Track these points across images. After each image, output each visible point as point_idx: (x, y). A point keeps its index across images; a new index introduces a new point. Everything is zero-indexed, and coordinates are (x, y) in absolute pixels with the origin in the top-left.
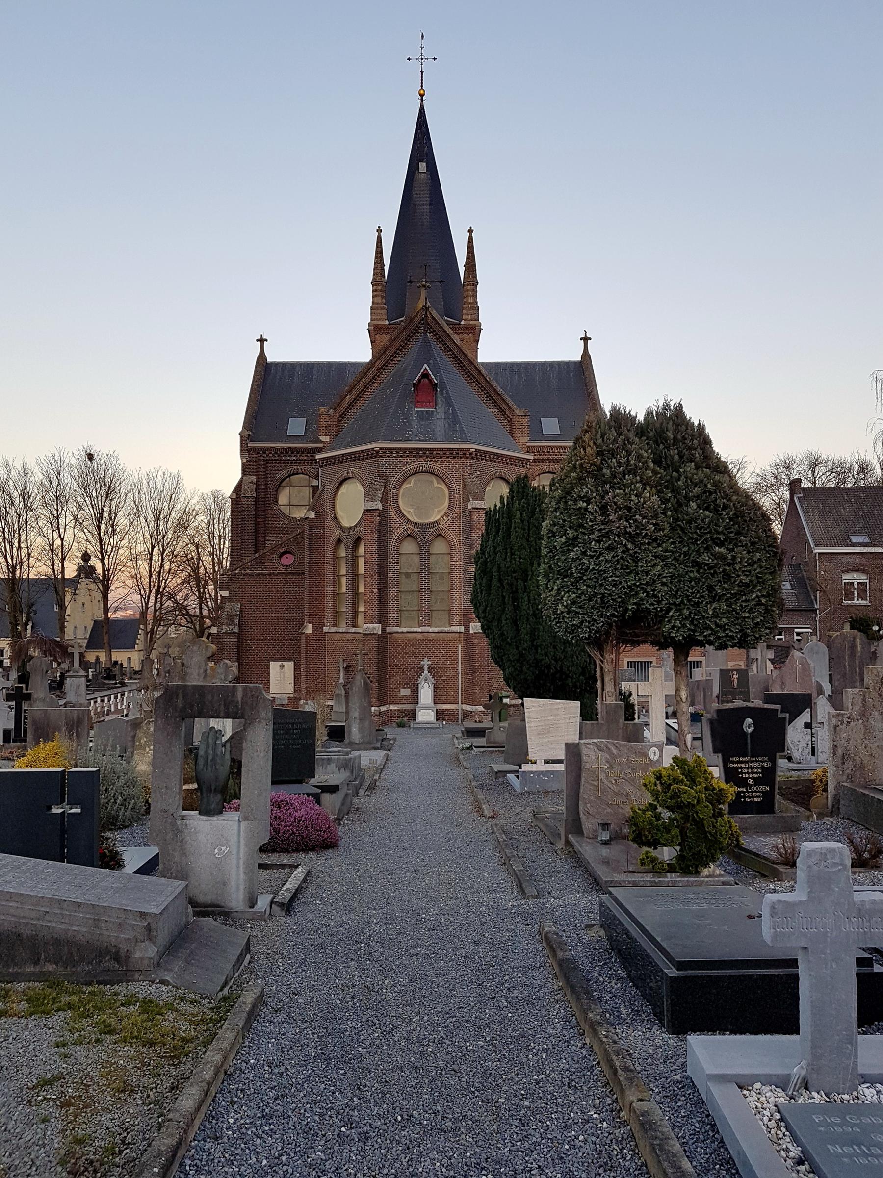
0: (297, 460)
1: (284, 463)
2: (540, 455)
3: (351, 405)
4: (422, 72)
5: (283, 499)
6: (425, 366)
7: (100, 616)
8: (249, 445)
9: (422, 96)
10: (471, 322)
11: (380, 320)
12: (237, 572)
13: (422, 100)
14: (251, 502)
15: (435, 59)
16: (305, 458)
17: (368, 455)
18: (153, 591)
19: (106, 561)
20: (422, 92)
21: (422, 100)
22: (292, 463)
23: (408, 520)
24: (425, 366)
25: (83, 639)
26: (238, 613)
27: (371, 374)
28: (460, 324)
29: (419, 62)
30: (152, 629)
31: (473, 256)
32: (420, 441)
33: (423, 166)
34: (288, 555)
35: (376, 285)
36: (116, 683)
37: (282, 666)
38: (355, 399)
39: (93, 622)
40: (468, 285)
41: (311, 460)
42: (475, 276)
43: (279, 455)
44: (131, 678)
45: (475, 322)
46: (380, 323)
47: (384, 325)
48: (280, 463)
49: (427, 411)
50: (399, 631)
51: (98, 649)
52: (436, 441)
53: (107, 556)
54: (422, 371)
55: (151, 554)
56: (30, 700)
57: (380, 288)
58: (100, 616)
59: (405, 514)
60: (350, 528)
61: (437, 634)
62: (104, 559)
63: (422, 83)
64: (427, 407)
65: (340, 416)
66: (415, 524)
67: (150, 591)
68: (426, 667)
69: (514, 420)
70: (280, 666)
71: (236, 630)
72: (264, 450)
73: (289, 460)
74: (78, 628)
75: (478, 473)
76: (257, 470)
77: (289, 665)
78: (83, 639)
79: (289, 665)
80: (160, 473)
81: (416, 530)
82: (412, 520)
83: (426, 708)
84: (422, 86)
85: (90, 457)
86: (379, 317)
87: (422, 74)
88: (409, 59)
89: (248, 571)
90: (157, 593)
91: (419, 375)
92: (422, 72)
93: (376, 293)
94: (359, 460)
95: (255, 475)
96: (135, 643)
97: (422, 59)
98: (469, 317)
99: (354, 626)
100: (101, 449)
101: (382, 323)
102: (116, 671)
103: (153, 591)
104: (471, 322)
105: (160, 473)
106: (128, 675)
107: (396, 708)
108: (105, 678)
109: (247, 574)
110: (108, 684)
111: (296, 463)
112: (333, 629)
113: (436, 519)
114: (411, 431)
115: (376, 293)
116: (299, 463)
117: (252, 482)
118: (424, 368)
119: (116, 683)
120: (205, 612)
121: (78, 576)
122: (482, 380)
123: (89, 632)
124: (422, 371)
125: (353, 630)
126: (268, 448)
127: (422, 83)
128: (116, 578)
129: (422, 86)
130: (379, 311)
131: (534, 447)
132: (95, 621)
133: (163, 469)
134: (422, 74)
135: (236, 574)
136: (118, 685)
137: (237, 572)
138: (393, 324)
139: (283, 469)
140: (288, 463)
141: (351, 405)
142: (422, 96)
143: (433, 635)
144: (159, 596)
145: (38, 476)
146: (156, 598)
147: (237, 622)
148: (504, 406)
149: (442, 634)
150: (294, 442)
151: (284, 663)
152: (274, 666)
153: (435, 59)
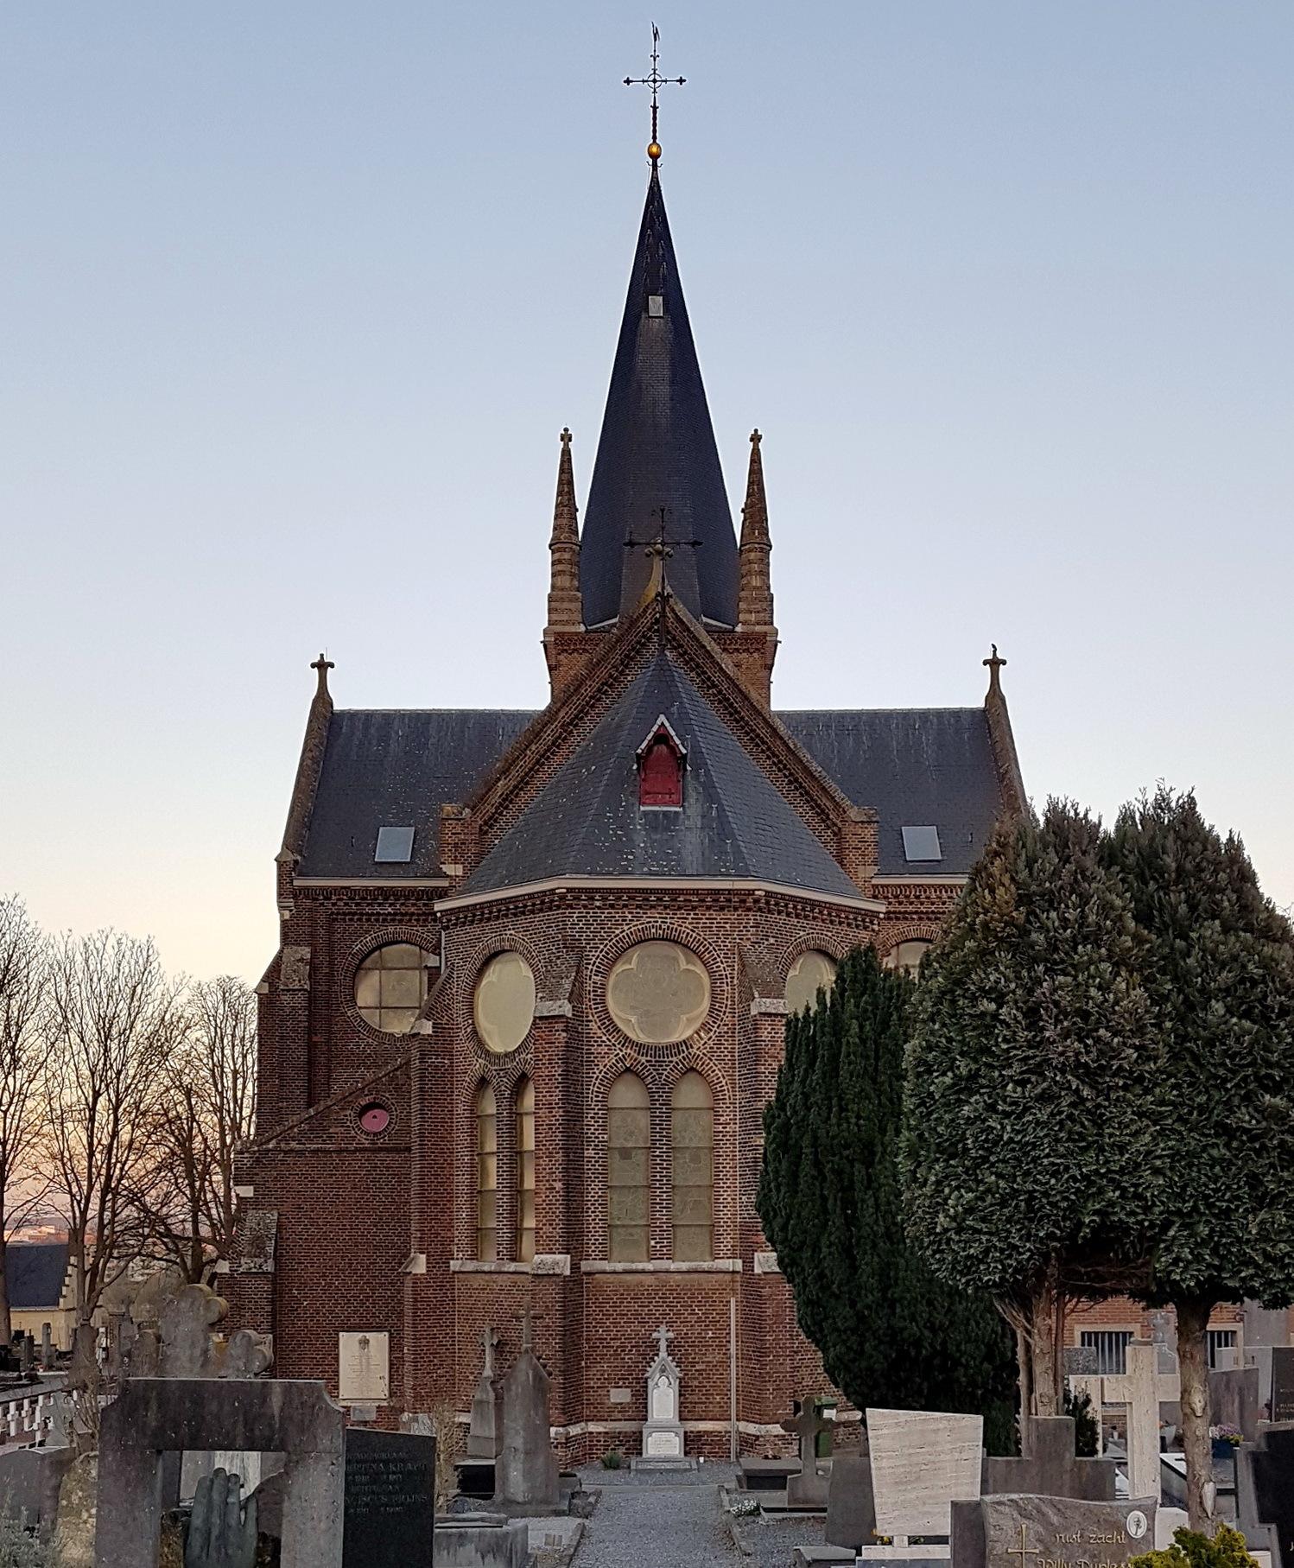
0: (395, 914)
1: (368, 920)
2: (900, 903)
3: (507, 800)
4: (655, 108)
5: (366, 994)
6: (662, 718)
8: (296, 883)
9: (655, 157)
10: (758, 628)
11: (567, 623)
13: (655, 166)
14: (300, 1000)
15: (628, 81)
16: (412, 910)
17: (543, 902)
18: (97, 1186)
20: (654, 149)
21: (655, 166)
23: (627, 1038)
24: (662, 718)
26: (274, 1231)
27: (548, 736)
28: (733, 631)
33: (656, 304)
34: (376, 1112)
35: (558, 550)
37: (365, 1343)
38: (515, 787)
40: (750, 551)
41: (424, 914)
43: (357, 904)
46: (567, 629)
47: (577, 634)
49: (665, 813)
50: (608, 1269)
52: (683, 875)
57: (567, 556)
59: (621, 1026)
60: (507, 1055)
61: (687, 1276)
63: (655, 131)
64: (666, 804)
65: (486, 823)
66: (641, 1048)
68: (663, 1345)
70: (360, 1342)
71: (269, 1267)
72: (328, 893)
73: (378, 914)
75: (772, 940)
76: (312, 935)
77: (379, 1341)
79: (379, 1341)
81: (643, 1059)
83: (664, 1428)
84: (654, 138)
86: (565, 617)
87: (655, 113)
88: (628, 81)
89: (293, 1145)
90: (106, 1189)
91: (649, 737)
92: (655, 108)
94: (523, 913)
95: (310, 945)
97: (655, 81)
98: (753, 617)
99: (513, 1260)
101: (573, 629)
103: (97, 1186)
107: (601, 1429)
109: (292, 1150)
111: (393, 920)
112: (471, 1266)
113: (684, 1037)
114: (632, 853)
115: (560, 567)
117: (301, 960)
118: (659, 722)
122: (779, 748)
124: (655, 728)
125: (512, 1267)
128: (19, 1158)
129: (654, 138)
130: (566, 605)
131: (887, 886)
134: (655, 113)
137: (271, 1146)
138: (595, 631)
139: (367, 932)
140: (377, 920)
141: (507, 800)
142: (655, 157)
143: (678, 1277)
146: (103, 1202)
147: (270, 1250)
149: (696, 1276)
150: (389, 877)
151: (368, 1335)
152: (348, 1342)
153: (681, 81)
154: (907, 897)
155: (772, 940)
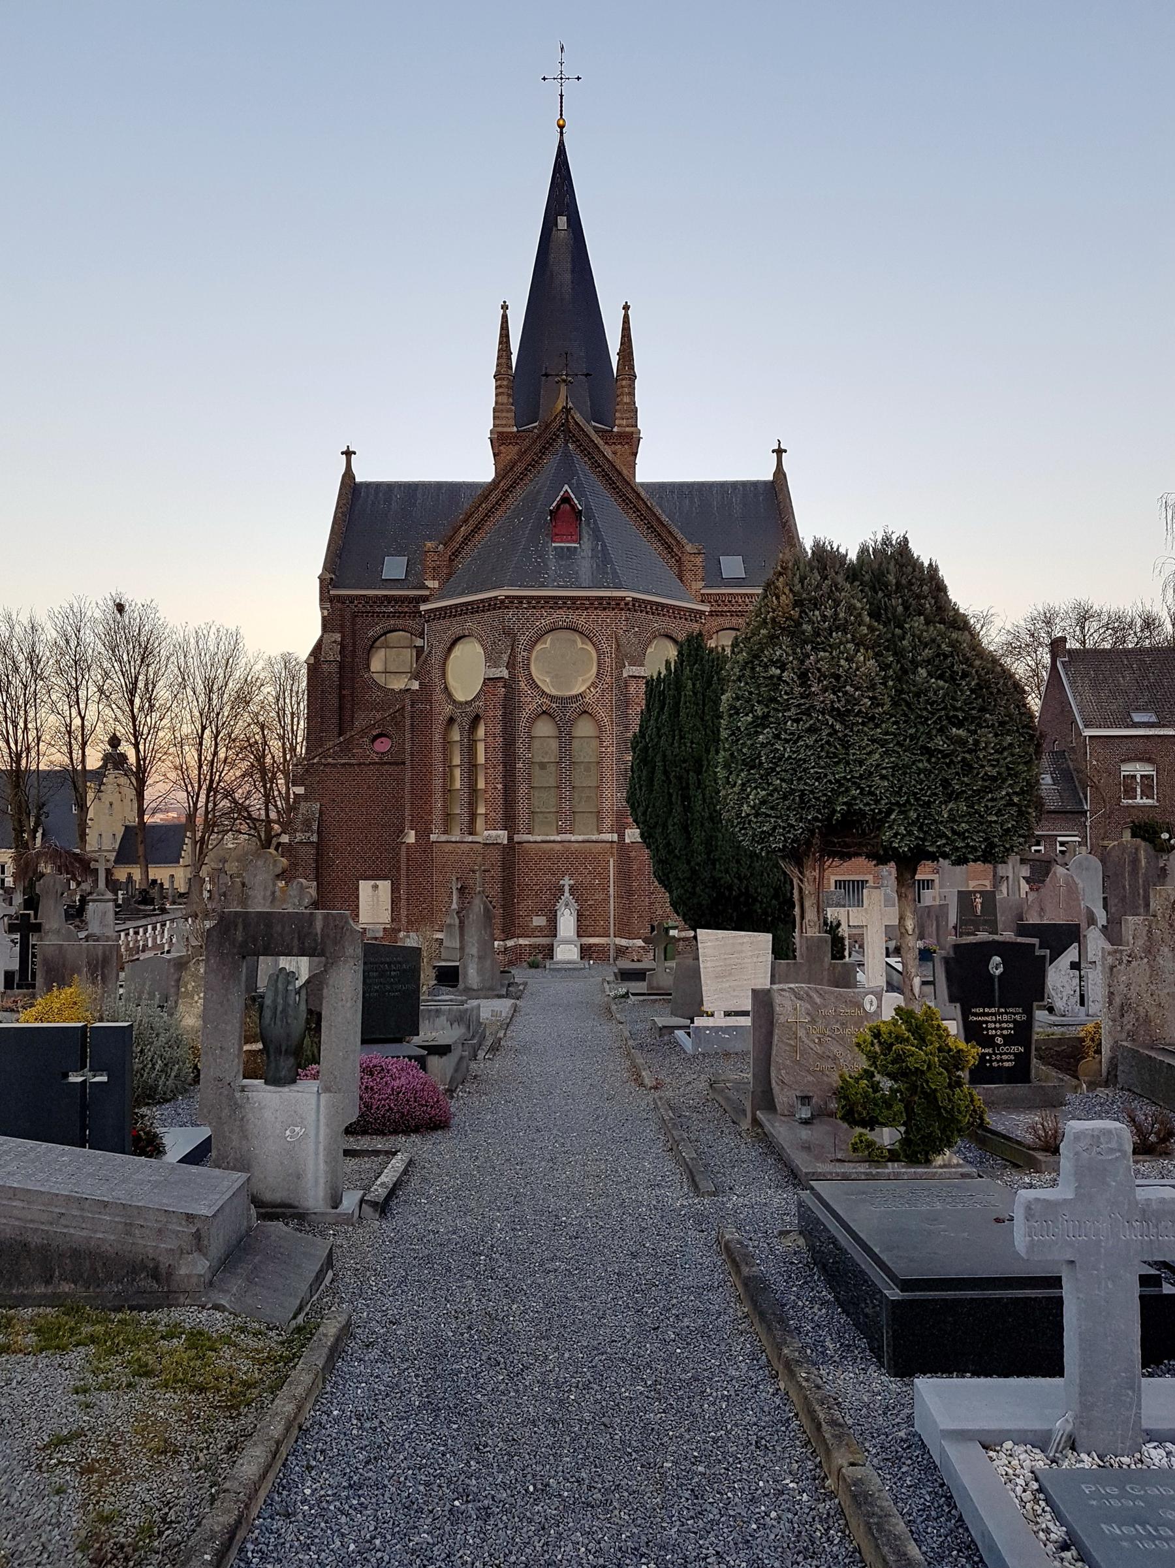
0: (395, 612)
1: (378, 616)
2: (719, 605)
3: (467, 539)
4: (561, 96)
7: (133, 820)
8: (331, 592)
9: (561, 127)
10: (627, 429)
11: (505, 426)
12: (315, 761)
13: (562, 133)
14: (334, 668)
15: (578, 78)
16: (406, 609)
19: (141, 747)
20: (561, 122)
21: (562, 133)
22: (388, 616)
23: (543, 692)
25: (110, 851)
26: (317, 815)
27: (493, 498)
28: (612, 431)
29: (557, 83)
30: (203, 838)
31: (630, 340)
32: (559, 586)
33: (562, 222)
34: (383, 739)
35: (500, 379)
36: (154, 910)
38: (472, 531)
39: (123, 828)
40: (623, 379)
41: (413, 612)
42: (632, 368)
43: (371, 606)
44: (174, 903)
45: (632, 429)
46: (505, 430)
47: (512, 433)
48: (372, 616)
51: (130, 864)
53: (142, 741)
54: (562, 493)
55: (201, 738)
56: (40, 931)
57: (505, 383)
58: (133, 820)
61: (582, 845)
62: (139, 743)
63: (561, 111)
65: (453, 554)
66: (553, 698)
67: (200, 787)
68: (567, 888)
69: (683, 559)
71: (314, 838)
72: (352, 599)
73: (384, 612)
74: (103, 836)
75: (637, 629)
76: (342, 626)
78: (110, 851)
80: (213, 629)
81: (554, 706)
82: (548, 692)
84: (561, 115)
85: (120, 608)
86: (504, 422)
87: (561, 99)
88: (544, 79)
89: (330, 760)
91: (558, 499)
92: (561, 96)
93: (500, 390)
95: (340, 632)
96: (180, 856)
97: (561, 78)
98: (624, 422)
100: (134, 597)
101: (509, 430)
102: (154, 892)
104: (627, 429)
105: (213, 629)
106: (170, 899)
108: (140, 903)
109: (329, 764)
110: (144, 910)
111: (394, 616)
115: (500, 390)
116: (398, 617)
117: (335, 642)
119: (154, 910)
120: (273, 815)
121: (104, 766)
122: (641, 506)
123: (119, 841)
124: (562, 493)
126: (357, 596)
127: (561, 111)
129: (561, 115)
130: (504, 414)
131: (711, 594)
132: (126, 827)
133: (217, 624)
134: (561, 99)
135: (314, 764)
136: (157, 912)
137: (315, 761)
138: (523, 431)
139: (377, 624)
140: (384, 616)
141: (467, 539)
142: (561, 127)
144: (212, 793)
145: (51, 633)
147: (315, 828)
148: (670, 540)
150: (391, 589)
153: (578, 78)
154: (723, 601)
155: (637, 629)
